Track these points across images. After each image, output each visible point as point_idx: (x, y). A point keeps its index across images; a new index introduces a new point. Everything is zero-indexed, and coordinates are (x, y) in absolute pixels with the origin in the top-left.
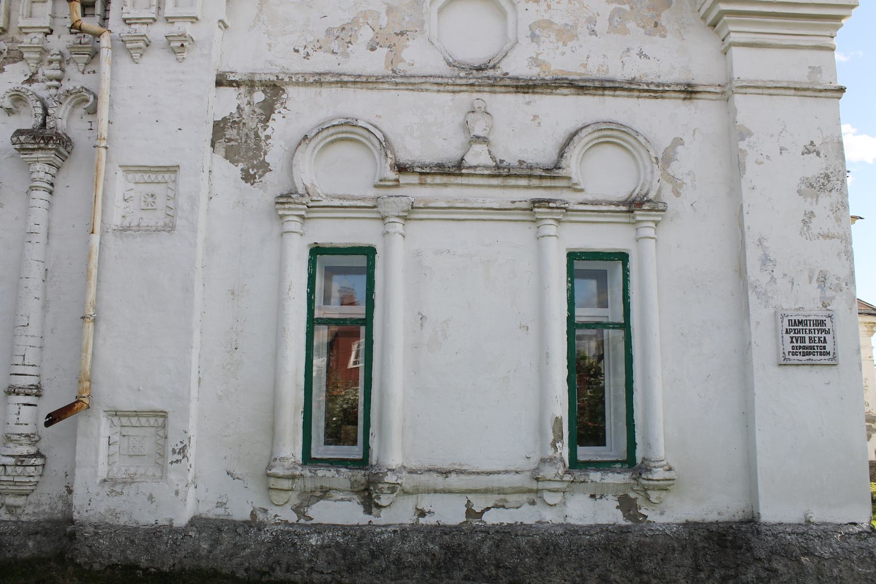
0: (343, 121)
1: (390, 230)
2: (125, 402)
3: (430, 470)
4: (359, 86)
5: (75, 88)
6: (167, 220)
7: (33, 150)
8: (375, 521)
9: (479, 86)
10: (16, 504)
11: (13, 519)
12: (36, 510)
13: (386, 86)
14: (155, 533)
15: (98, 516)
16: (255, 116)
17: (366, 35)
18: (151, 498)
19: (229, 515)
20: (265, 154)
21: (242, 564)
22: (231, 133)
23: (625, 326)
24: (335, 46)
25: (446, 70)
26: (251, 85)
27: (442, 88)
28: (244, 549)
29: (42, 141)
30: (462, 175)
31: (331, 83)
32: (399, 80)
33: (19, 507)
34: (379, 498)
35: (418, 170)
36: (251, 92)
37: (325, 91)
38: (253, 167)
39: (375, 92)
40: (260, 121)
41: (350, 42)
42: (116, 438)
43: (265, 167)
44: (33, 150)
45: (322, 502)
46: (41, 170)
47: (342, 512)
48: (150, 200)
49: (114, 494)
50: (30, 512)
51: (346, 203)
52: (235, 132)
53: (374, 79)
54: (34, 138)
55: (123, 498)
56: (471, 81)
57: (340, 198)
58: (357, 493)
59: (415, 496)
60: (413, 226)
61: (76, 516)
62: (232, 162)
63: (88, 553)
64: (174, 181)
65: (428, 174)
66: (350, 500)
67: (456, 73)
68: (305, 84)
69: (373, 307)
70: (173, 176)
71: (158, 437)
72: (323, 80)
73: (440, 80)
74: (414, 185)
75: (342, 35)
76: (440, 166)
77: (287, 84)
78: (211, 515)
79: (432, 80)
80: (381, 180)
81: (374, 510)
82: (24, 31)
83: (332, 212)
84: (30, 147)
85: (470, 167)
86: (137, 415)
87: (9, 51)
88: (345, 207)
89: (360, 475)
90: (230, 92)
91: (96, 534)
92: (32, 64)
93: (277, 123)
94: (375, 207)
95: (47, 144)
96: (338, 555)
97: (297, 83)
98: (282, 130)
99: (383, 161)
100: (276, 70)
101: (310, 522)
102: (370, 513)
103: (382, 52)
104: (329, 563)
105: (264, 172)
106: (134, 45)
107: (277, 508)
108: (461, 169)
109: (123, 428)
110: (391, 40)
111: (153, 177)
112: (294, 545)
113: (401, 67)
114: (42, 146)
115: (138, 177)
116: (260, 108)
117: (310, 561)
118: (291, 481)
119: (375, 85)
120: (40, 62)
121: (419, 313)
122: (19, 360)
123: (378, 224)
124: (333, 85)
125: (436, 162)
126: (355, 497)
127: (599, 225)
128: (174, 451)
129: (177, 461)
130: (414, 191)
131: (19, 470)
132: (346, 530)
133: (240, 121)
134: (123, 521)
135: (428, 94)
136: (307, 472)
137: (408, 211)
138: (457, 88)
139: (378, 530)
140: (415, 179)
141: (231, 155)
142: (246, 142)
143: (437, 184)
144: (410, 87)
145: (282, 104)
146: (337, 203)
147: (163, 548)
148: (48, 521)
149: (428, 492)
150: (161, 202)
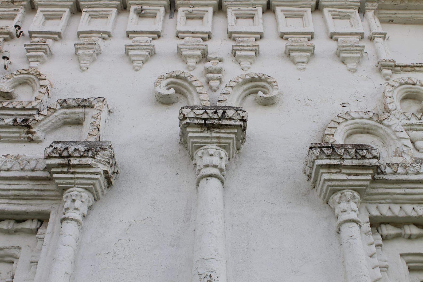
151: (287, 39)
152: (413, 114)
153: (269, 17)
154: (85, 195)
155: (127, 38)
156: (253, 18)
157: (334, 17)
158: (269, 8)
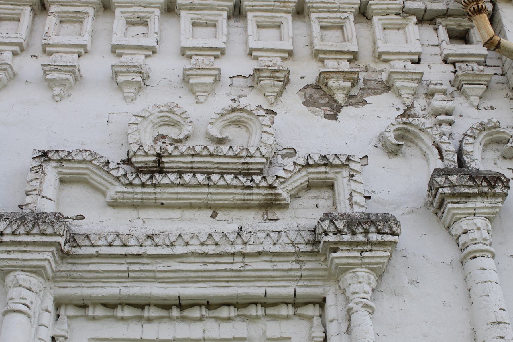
7: (468, 196)
29: (485, 184)
44: (468, 196)
82: (384, 57)
84: (467, 190)
95: (493, 187)
114: (486, 189)
120: (415, 95)
151: (256, 58)
152: (336, 155)
153: (236, 26)
155: (248, 57)
156: (279, 27)
157: (62, 19)
158: (237, 13)
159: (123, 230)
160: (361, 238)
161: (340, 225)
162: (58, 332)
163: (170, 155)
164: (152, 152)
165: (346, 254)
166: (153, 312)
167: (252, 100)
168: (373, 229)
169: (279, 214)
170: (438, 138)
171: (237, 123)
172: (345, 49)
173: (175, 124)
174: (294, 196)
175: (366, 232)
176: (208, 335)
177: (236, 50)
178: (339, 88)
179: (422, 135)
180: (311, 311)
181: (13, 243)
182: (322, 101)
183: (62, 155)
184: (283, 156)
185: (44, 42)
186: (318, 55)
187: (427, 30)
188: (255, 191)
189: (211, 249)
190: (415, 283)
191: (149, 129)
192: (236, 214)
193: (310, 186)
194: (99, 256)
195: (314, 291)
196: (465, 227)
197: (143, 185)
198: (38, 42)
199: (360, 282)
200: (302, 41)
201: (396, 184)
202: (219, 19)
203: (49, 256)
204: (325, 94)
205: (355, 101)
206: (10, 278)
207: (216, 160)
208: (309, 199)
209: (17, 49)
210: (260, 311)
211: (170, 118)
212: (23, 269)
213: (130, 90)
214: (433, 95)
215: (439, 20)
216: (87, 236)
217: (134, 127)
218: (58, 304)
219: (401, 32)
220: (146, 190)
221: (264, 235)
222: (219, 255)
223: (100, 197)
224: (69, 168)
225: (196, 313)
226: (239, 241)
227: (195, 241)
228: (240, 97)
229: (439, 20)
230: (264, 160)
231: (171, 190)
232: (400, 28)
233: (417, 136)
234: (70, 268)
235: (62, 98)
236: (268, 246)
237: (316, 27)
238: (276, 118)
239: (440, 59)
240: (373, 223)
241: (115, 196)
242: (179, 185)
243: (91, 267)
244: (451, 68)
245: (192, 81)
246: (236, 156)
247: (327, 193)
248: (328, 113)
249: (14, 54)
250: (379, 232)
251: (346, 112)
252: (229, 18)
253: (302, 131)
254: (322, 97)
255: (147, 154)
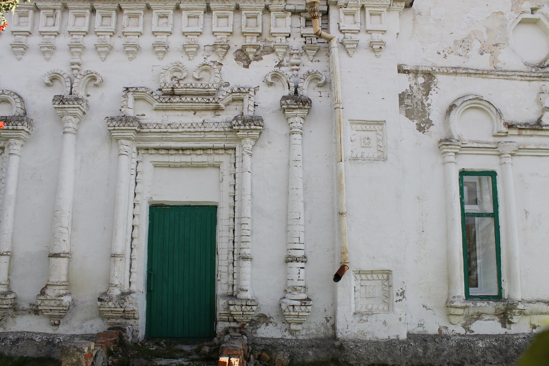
0: (475, 97)
1: (507, 162)
2: (366, 266)
3: (538, 301)
4: (477, 76)
5: (313, 70)
6: (380, 154)
7: (294, 109)
8: (509, 332)
9: (544, 77)
10: (297, 329)
11: (294, 338)
12: (307, 333)
13: (492, 76)
14: (391, 344)
15: (353, 335)
16: (420, 92)
17: (476, 46)
18: (385, 323)
19: (425, 331)
20: (429, 115)
21: (445, 360)
22: (408, 101)
23: (495, 215)
24: (460, 51)
25: (524, 68)
26: (416, 73)
27: (523, 78)
28: (443, 351)
30: (542, 130)
31: (462, 73)
32: (500, 73)
33: (298, 331)
34: (512, 318)
35: (519, 127)
36: (416, 77)
37: (458, 78)
38: (423, 122)
39: (486, 80)
40: (423, 95)
41: (468, 49)
42: (358, 287)
43: (430, 123)
44: (294, 109)
45: (478, 321)
46: (297, 121)
47: (489, 327)
48: (367, 141)
49: (362, 321)
50: (304, 334)
51: (481, 146)
52: (409, 101)
53: (486, 72)
54: (296, 102)
55: (368, 323)
56: (540, 75)
57: (478, 142)
58: (497, 315)
59: (529, 316)
60: (516, 159)
61: (339, 335)
62: (411, 119)
63: (355, 358)
64: (381, 130)
65: (523, 129)
66: (493, 320)
67: (530, 70)
68: (448, 73)
69: (498, 206)
70: (380, 127)
71: (384, 286)
72: (458, 71)
73: (522, 74)
74: (514, 135)
75: (463, 45)
76: (526, 124)
77: (437, 73)
78: (415, 332)
79: (518, 73)
80: (498, 132)
81: (507, 325)
82: (273, 35)
83: (472, 150)
84: (293, 107)
85: (546, 126)
86: (372, 273)
87: (264, 47)
88: (479, 148)
89: (501, 305)
90: (404, 76)
91: (357, 346)
92: (280, 55)
93: (433, 97)
94: (497, 148)
95: (304, 105)
96: (498, 353)
97: (443, 73)
98: (437, 102)
99: (499, 121)
100: (429, 64)
101: (472, 334)
102: (505, 327)
103: (487, 56)
104: (494, 358)
105: (430, 126)
106: (351, 46)
107: (453, 326)
108: (542, 127)
109: (362, 281)
110: (491, 48)
111: (368, 127)
112: (470, 347)
113: (499, 65)
114: (301, 106)
115: (359, 127)
116: (422, 87)
117: (483, 357)
118: (463, 310)
119: (486, 76)
120: (285, 54)
121: (525, 210)
122: (297, 240)
123: (497, 158)
124: (463, 75)
125: (524, 122)
126: (496, 318)
127: (544, 158)
128: (397, 294)
129: (400, 300)
130: (518, 140)
131: (303, 308)
132: (497, 337)
133: (412, 94)
134: (368, 337)
135: (516, 82)
136: (470, 304)
137: (516, 151)
138: (532, 79)
139: (516, 337)
140: (515, 132)
141: (409, 114)
142: (416, 107)
143: (527, 135)
144: (506, 77)
145: (435, 85)
146: (475, 145)
147: (399, 353)
148: (316, 339)
149: (537, 314)
150: (374, 143)
154: (253, 142)
159: (159, 122)
160: (247, 127)
161: (240, 122)
162: (139, 160)
163: (177, 88)
164: (170, 87)
165: (242, 133)
166: (173, 152)
167: (214, 57)
168: (252, 123)
169: (220, 113)
170: (288, 79)
171: (206, 70)
172: (256, 32)
173: (180, 71)
174: (227, 105)
175: (250, 125)
176: (193, 160)
177: (208, 31)
178: (250, 52)
179: (283, 77)
180: (231, 152)
181: (119, 129)
182: (243, 58)
183: (134, 89)
184: (224, 86)
185: (123, 31)
186: (244, 34)
187: (296, 19)
188: (211, 104)
189: (192, 130)
190: (270, 143)
191: (169, 75)
192: (203, 113)
193: (234, 100)
194: (151, 132)
195: (232, 145)
196: (292, 121)
197: (166, 102)
198: (120, 30)
199: (248, 143)
200: (237, 25)
201: (269, 99)
202: (200, 14)
203: (132, 134)
204: (245, 54)
205: (258, 58)
206: (119, 141)
207: (196, 90)
208: (233, 106)
209: (111, 34)
210: (212, 152)
211: (178, 68)
212: (124, 138)
213: (161, 55)
214: (292, 55)
215: (302, 14)
216: (146, 124)
217: (162, 74)
218: (138, 149)
219: (284, 19)
220: (167, 104)
221: (212, 124)
222: (195, 132)
223: (150, 106)
224: (137, 95)
225: (188, 152)
226: (203, 126)
227: (186, 127)
228: (208, 56)
229: (302, 14)
230: (215, 90)
231: (177, 104)
232: (284, 17)
233: (281, 77)
234: (141, 136)
235: (133, 59)
236: (214, 129)
237: (244, 18)
238: (223, 67)
239: (300, 35)
240: (253, 121)
241: (156, 107)
242: (180, 102)
243: (148, 136)
244: (304, 39)
245: (187, 50)
246: (204, 88)
247: (240, 103)
248: (245, 64)
249: (111, 36)
250: (255, 125)
251: (254, 63)
252: (205, 12)
253: (234, 74)
254: (244, 57)
255: (168, 88)
